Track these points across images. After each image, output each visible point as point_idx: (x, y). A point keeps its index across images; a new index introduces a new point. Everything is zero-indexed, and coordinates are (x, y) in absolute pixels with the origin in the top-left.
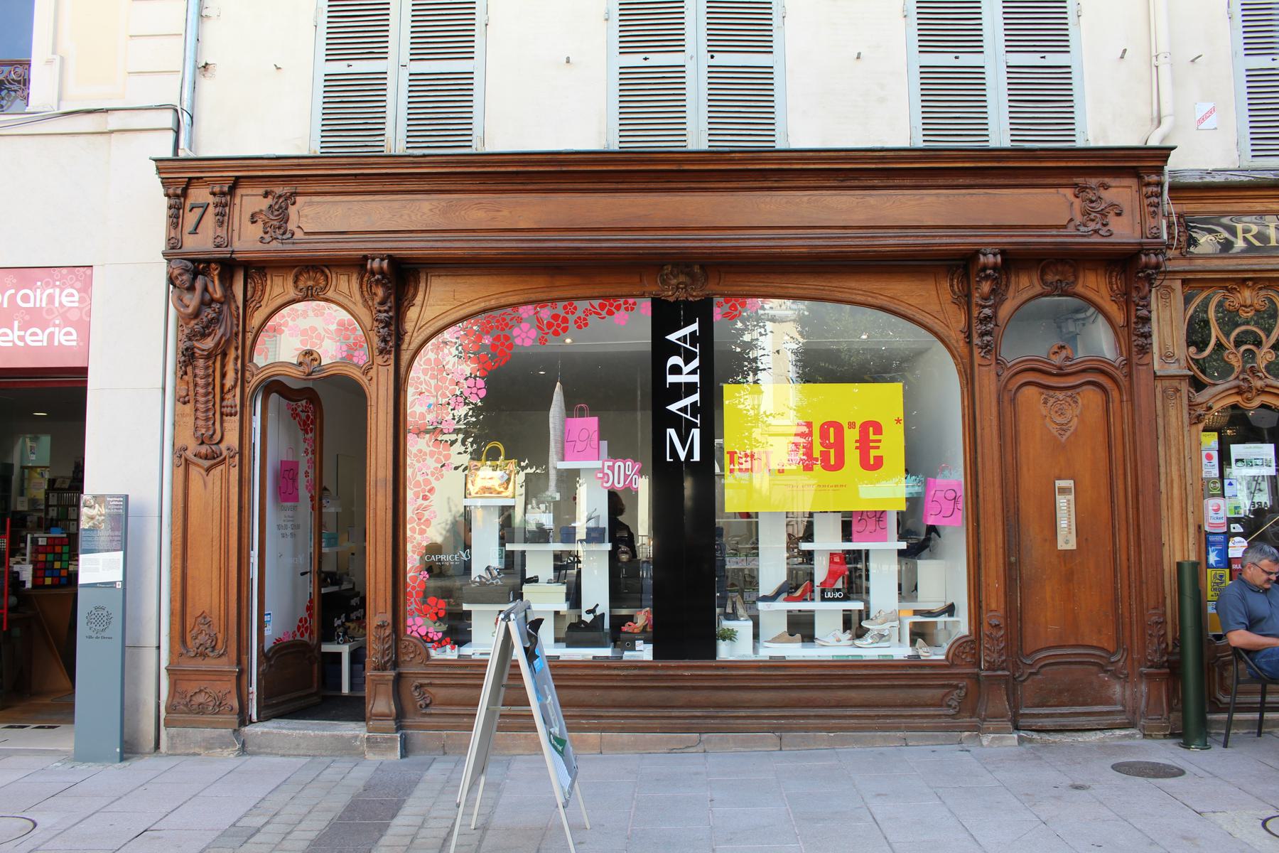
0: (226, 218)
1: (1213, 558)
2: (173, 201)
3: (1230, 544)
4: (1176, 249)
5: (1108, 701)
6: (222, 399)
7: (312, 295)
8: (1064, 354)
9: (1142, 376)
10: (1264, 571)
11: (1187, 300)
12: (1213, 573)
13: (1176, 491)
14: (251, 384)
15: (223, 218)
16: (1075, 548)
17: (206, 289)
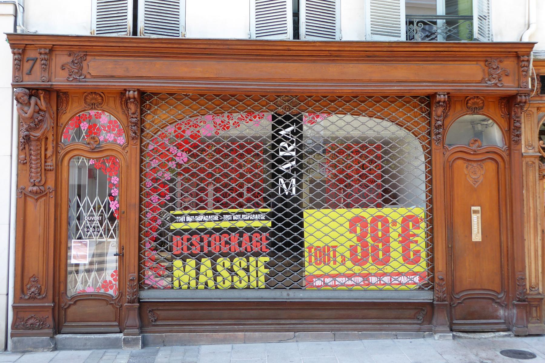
0: (48, 66)
2: (16, 56)
5: (497, 318)
6: (45, 162)
7: (95, 108)
8: (477, 144)
13: (532, 214)
14: (61, 154)
15: (46, 67)
17: (36, 104)
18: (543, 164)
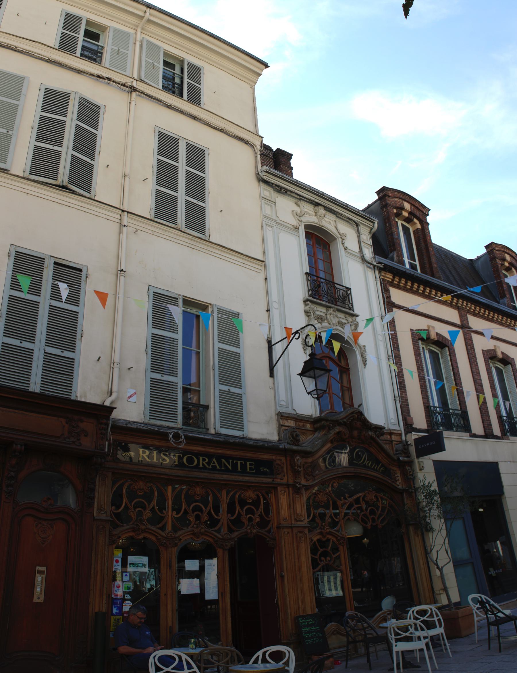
1: (115, 611)
3: (124, 604)
4: (111, 457)
10: (138, 617)
11: (113, 484)
12: (114, 618)
16: (42, 601)
18: (113, 530)
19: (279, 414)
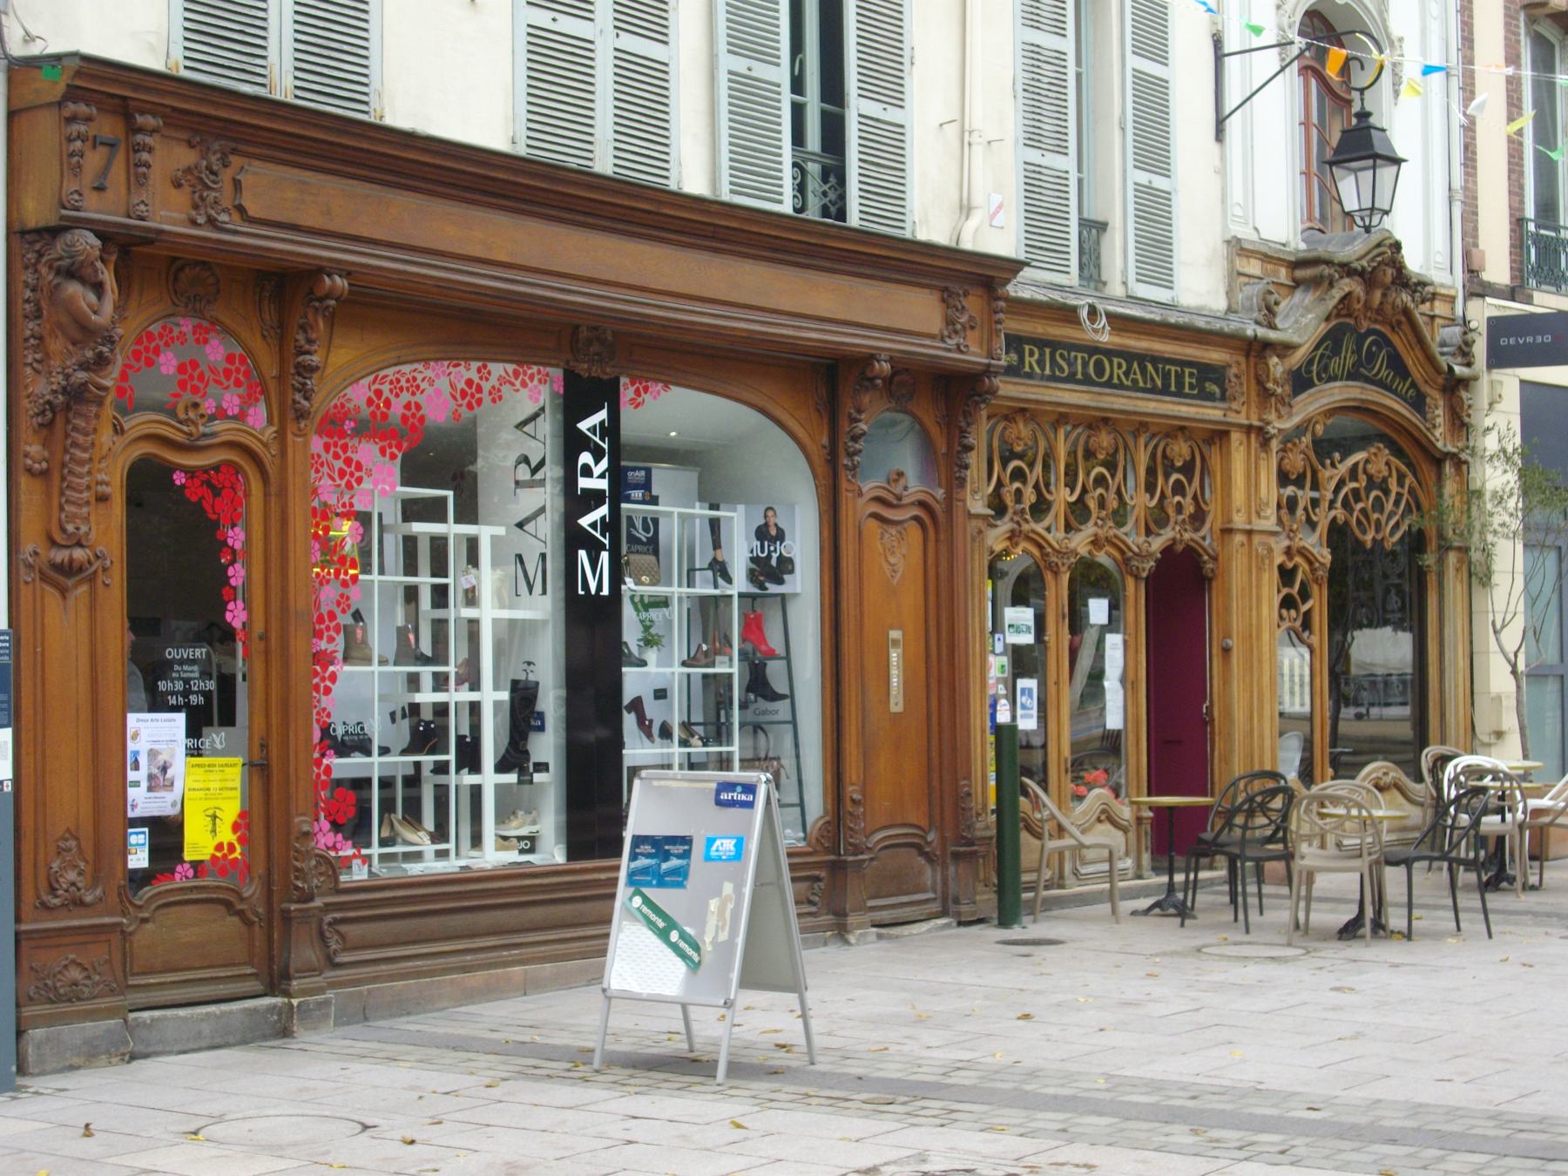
9: (959, 517)
19: (1234, 243)
